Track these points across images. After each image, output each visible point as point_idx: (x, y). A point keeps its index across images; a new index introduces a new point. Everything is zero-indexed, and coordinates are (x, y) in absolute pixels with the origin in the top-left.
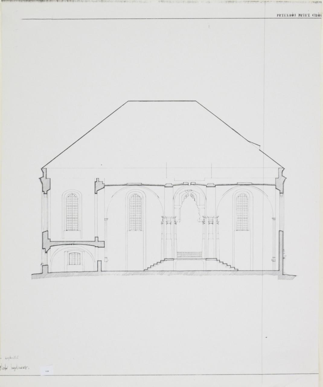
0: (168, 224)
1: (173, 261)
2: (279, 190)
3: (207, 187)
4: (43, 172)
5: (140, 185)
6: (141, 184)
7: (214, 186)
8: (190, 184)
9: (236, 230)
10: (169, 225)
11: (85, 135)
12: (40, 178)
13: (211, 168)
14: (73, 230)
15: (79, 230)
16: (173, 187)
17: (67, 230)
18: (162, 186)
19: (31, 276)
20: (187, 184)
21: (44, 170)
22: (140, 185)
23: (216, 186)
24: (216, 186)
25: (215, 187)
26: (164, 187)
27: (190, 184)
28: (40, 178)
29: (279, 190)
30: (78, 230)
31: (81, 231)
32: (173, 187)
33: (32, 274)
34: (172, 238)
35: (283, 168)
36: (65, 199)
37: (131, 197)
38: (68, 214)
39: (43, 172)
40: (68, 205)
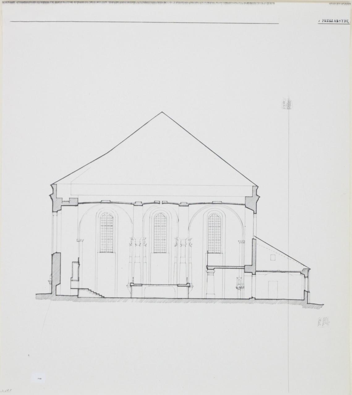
0: (137, 246)
1: (141, 287)
2: (253, 210)
3: (179, 206)
4: (53, 188)
5: (220, 204)
6: (109, 202)
7: (187, 205)
8: (161, 203)
9: (99, 252)
10: (138, 247)
11: (205, 146)
12: (50, 195)
13: (71, 184)
14: (161, 253)
15: (114, 252)
16: (142, 205)
17: (100, 252)
18: (150, 203)
19: (35, 296)
20: (159, 202)
21: (54, 186)
22: (220, 204)
23: (189, 205)
24: (189, 205)
25: (188, 206)
26: (178, 205)
27: (161, 203)
28: (50, 195)
29: (253, 210)
30: (112, 252)
31: (170, 254)
32: (188, 206)
33: (36, 294)
34: (141, 262)
35: (257, 186)
36: (153, 218)
37: (102, 215)
38: (165, 236)
39: (53, 188)
40: (156, 225)
